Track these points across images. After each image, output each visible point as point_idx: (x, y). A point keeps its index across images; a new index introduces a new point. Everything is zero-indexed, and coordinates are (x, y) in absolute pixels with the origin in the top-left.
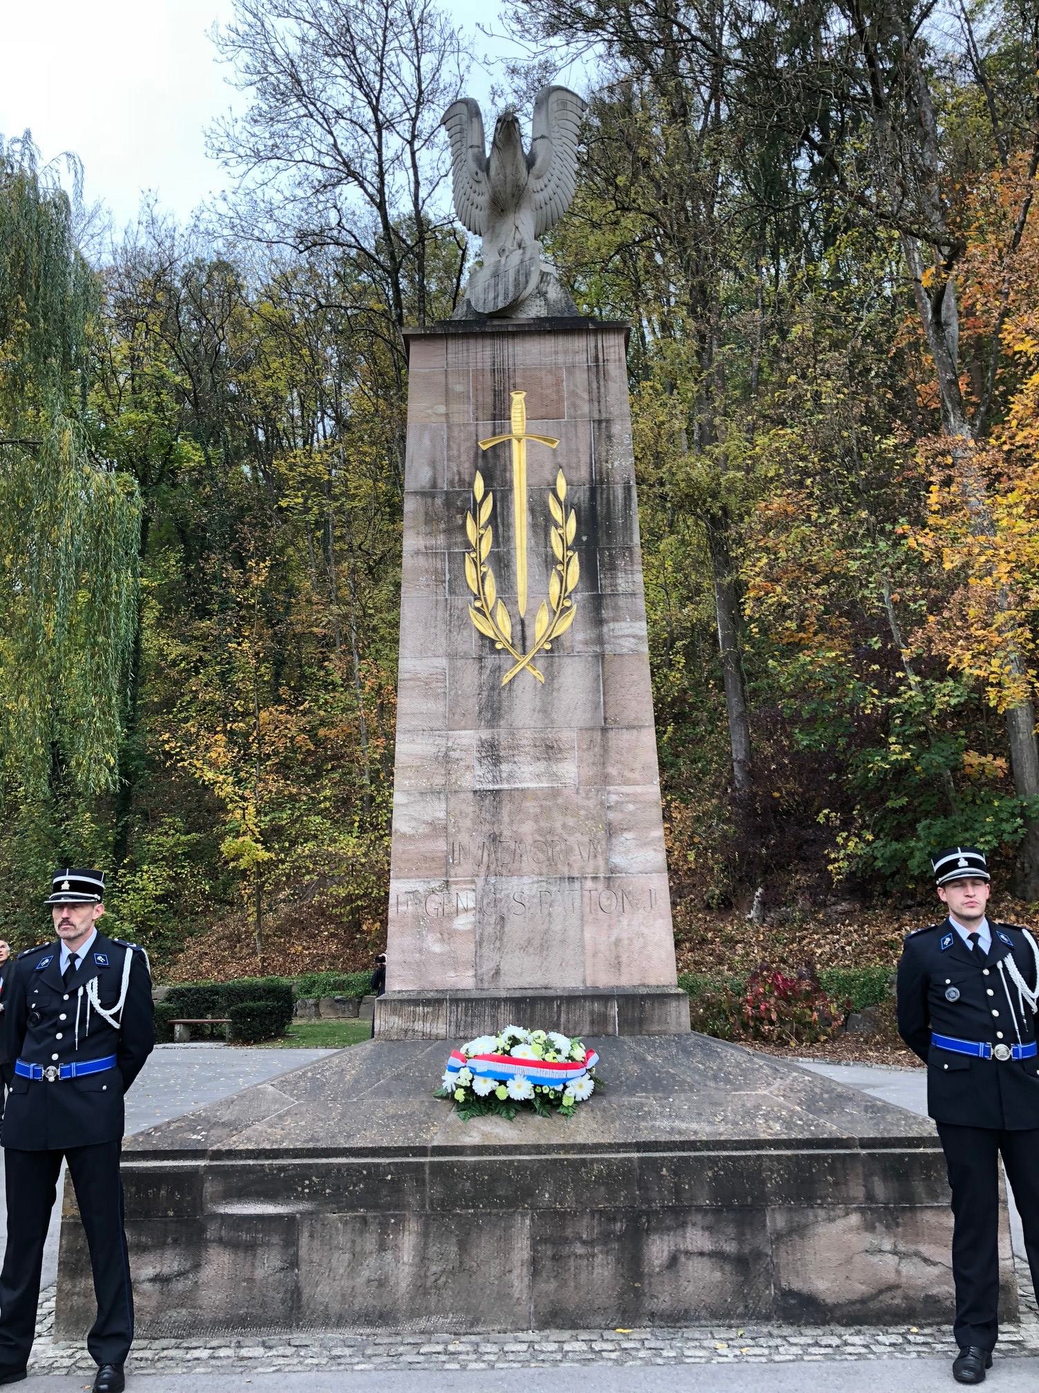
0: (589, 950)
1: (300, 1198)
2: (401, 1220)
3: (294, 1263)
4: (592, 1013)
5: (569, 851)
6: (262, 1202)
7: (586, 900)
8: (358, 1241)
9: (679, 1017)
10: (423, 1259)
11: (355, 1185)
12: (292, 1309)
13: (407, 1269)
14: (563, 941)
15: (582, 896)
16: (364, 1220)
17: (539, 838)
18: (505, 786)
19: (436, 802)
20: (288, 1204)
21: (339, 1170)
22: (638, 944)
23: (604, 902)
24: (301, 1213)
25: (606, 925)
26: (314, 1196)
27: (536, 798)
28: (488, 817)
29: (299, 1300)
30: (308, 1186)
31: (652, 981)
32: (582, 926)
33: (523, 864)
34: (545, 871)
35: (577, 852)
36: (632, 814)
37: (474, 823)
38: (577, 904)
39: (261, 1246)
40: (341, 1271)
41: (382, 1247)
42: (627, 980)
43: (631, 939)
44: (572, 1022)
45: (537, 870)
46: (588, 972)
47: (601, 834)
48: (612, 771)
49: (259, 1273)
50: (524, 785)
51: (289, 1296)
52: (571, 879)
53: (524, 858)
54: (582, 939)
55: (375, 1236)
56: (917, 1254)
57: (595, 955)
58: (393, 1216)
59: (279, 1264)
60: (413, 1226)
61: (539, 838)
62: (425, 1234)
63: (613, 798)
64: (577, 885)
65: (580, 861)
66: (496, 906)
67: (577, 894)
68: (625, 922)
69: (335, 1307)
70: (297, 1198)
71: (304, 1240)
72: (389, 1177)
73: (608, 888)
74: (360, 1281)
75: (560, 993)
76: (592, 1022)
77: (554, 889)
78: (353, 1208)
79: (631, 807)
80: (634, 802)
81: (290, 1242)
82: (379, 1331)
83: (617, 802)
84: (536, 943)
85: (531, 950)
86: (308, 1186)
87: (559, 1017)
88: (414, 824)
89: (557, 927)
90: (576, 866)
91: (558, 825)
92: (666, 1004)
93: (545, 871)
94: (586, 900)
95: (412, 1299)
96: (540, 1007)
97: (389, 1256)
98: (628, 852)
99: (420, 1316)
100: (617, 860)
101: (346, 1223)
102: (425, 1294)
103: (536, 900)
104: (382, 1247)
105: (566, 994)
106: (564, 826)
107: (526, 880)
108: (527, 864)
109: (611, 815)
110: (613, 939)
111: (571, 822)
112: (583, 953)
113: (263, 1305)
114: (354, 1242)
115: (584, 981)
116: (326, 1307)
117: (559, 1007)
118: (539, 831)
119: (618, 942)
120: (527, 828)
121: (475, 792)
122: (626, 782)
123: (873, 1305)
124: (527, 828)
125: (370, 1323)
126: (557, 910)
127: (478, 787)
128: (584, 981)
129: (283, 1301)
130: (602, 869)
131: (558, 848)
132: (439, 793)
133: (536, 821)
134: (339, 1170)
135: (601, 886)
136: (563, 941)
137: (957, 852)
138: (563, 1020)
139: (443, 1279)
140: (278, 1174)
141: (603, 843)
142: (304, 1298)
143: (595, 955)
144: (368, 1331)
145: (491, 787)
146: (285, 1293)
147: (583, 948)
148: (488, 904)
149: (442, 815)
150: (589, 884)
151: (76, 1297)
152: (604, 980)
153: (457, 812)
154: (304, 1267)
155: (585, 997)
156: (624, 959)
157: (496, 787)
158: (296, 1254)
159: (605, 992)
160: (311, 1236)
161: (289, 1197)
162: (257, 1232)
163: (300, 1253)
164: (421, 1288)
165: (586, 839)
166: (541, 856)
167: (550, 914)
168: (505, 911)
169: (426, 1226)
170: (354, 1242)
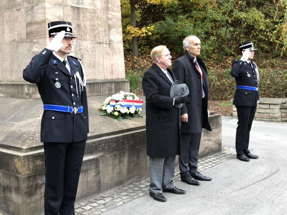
0: (105, 67)
1: (99, 152)
2: (124, 153)
3: (98, 173)
4: (108, 87)
5: (99, 33)
6: (89, 155)
7: (104, 50)
8: (114, 161)
9: (127, 88)
10: (129, 163)
11: (113, 144)
12: (99, 187)
13: (126, 167)
14: (99, 64)
15: (103, 49)
16: (116, 155)
17: (91, 28)
18: (81, 6)
19: (60, 9)
20: (96, 154)
21: (109, 140)
22: (117, 66)
23: (109, 52)
24: (99, 157)
25: (109, 59)
26: (103, 150)
27: (90, 13)
28: (76, 18)
29: (100, 184)
30: (101, 147)
31: (120, 77)
32: (103, 59)
33: (87, 37)
34: (93, 39)
35: (101, 34)
36: (115, 22)
37: (72, 19)
38: (102, 52)
39: (89, 170)
40: (110, 172)
41: (120, 162)
42: (114, 77)
43: (115, 64)
44: (103, 90)
45: (91, 39)
46: (105, 75)
47: (107, 28)
48: (110, 6)
49: (89, 179)
50: (85, 7)
51: (98, 184)
52: (100, 43)
53: (87, 34)
54: (103, 64)
55: (118, 159)
56: (210, 140)
57: (107, 69)
58: (122, 152)
59: (94, 174)
60: (127, 154)
61: (91, 28)
62: (129, 156)
63: (110, 16)
64: (102, 45)
65: (102, 38)
66: (80, 51)
67: (102, 48)
68: (114, 59)
69: (109, 183)
70: (98, 152)
71: (101, 165)
72: (121, 140)
73: (109, 47)
74: (115, 173)
75: (100, 81)
76: (108, 90)
77: (96, 46)
78: (113, 152)
79: (114, 20)
80: (115, 18)
81: (97, 167)
82: (120, 187)
83: (111, 18)
84: (92, 64)
85: (91, 67)
86: (101, 147)
87: (100, 89)
88: (53, 17)
89: (97, 59)
90: (101, 38)
91: (96, 23)
92: (124, 84)
93: (93, 39)
94: (104, 50)
95: (127, 175)
96: (95, 86)
97: (122, 164)
98: (114, 35)
99: (129, 180)
100: (112, 38)
101: (111, 157)
102: (130, 173)
103: (91, 50)
104: (120, 162)
105: (102, 82)
106: (98, 24)
107: (88, 42)
108: (88, 37)
109: (110, 22)
110: (111, 64)
111: (99, 23)
112: (104, 69)
113: (91, 188)
114: (113, 162)
115: (104, 78)
116: (107, 184)
117: (100, 86)
118: (91, 25)
119: (112, 65)
120: (88, 23)
121: (72, 7)
122: (113, 11)
123: (205, 153)
124: (88, 23)
125: (118, 185)
126: (97, 53)
127: (72, 5)
128: (104, 78)
129: (96, 185)
130: (108, 40)
131: (96, 32)
132: (61, 5)
133: (90, 21)
134: (109, 140)
135: (108, 46)
136: (99, 64)
137: (251, 43)
138: (101, 90)
139: (134, 168)
140: (93, 145)
141: (108, 31)
142: (102, 183)
143: (107, 69)
144: (117, 188)
145: (76, 6)
146: (97, 183)
147: (104, 66)
148: (78, 50)
149: (62, 14)
150: (105, 45)
151: (32, 204)
152: (109, 77)
153: (67, 14)
154: (101, 173)
155: (106, 82)
156: (114, 70)
157: (78, 6)
158: (99, 170)
159: (111, 81)
160: (102, 163)
161: (96, 152)
162: (88, 165)
163: (100, 169)
164: (129, 171)
165: (103, 30)
166: (92, 34)
167: (95, 55)
168: (83, 53)
169: (130, 153)
170: (113, 162)
